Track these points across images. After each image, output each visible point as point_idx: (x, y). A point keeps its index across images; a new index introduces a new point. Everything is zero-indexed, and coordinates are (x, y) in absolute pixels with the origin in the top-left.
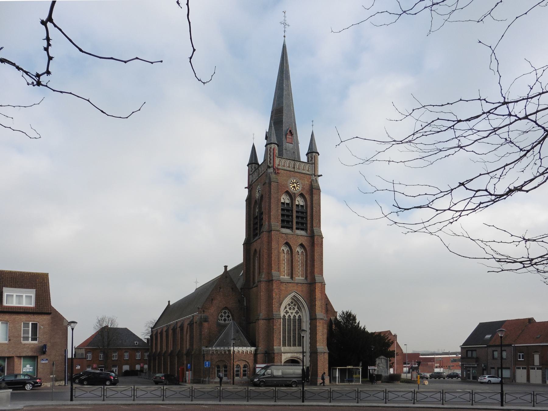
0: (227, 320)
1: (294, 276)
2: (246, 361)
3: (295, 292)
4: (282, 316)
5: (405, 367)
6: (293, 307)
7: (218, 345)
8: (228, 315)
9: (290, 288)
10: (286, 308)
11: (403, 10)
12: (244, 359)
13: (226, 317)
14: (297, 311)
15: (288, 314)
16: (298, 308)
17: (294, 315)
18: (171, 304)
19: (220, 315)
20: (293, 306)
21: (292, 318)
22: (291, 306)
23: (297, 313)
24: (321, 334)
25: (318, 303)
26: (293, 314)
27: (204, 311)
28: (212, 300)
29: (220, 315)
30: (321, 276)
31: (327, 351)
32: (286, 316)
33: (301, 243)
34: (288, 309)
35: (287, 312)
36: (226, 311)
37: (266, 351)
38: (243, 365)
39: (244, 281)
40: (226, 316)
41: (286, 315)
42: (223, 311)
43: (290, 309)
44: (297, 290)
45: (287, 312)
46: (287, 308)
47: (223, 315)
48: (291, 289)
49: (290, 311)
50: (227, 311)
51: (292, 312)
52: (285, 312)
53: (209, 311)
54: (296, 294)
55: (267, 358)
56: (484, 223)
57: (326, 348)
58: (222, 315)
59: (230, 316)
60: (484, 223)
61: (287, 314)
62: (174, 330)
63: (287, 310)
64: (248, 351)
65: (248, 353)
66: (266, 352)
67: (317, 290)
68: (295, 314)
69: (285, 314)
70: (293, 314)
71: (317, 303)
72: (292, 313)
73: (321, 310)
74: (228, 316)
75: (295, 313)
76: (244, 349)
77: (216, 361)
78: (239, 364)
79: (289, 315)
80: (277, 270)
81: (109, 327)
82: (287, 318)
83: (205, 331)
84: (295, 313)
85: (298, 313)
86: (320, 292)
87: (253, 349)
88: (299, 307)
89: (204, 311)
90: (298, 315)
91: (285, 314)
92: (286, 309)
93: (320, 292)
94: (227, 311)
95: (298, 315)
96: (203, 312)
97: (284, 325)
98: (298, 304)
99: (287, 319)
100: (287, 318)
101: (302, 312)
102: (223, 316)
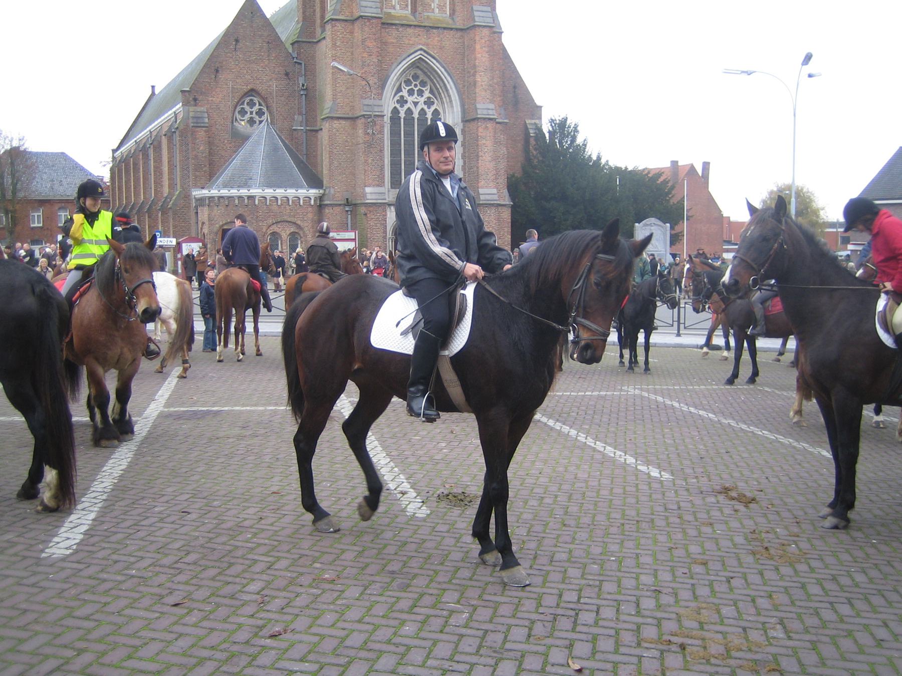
0: (258, 122)
1: (420, 9)
2: (295, 223)
3: (421, 49)
4: (388, 113)
5: (728, 251)
7: (226, 186)
8: (260, 109)
9: (409, 40)
10: (399, 90)
11: (552, 605)
12: (289, 219)
13: (254, 115)
14: (429, 98)
15: (406, 107)
16: (431, 92)
17: (422, 109)
18: (157, 92)
19: (238, 109)
20: (419, 87)
21: (416, 115)
22: (413, 87)
23: (429, 103)
24: (490, 158)
25: (482, 79)
26: (419, 107)
27: (195, 100)
28: (217, 71)
29: (238, 109)
30: (489, 9)
31: (507, 201)
34: (404, 93)
35: (402, 101)
36: (255, 99)
37: (347, 199)
38: (288, 233)
39: (300, 25)
40: (254, 113)
41: (400, 109)
42: (247, 100)
43: (411, 92)
44: (427, 45)
45: (402, 101)
46: (403, 90)
47: (247, 108)
48: (411, 42)
49: (410, 99)
50: (256, 100)
51: (416, 100)
52: (398, 101)
54: (426, 55)
55: (349, 216)
56: (727, 72)
57: (505, 192)
58: (243, 108)
59: (264, 113)
60: (727, 72)
61: (402, 106)
63: (402, 97)
64: (299, 199)
65: (299, 202)
66: (347, 202)
67: (478, 47)
68: (425, 107)
69: (398, 106)
70: (419, 107)
71: (478, 79)
72: (416, 104)
74: (260, 113)
75: (425, 103)
76: (291, 192)
77: (221, 223)
78: (278, 230)
79: (409, 109)
82: (402, 115)
83: (198, 149)
84: (425, 103)
85: (433, 103)
86: (486, 49)
87: (313, 192)
88: (434, 89)
89: (195, 100)
90: (433, 108)
91: (398, 106)
92: (400, 94)
93: (486, 49)
94: (256, 100)
95: (433, 108)
96: (192, 103)
97: (395, 133)
98: (432, 80)
99: (402, 120)
100: (402, 115)
101: (442, 103)
102: (246, 113)
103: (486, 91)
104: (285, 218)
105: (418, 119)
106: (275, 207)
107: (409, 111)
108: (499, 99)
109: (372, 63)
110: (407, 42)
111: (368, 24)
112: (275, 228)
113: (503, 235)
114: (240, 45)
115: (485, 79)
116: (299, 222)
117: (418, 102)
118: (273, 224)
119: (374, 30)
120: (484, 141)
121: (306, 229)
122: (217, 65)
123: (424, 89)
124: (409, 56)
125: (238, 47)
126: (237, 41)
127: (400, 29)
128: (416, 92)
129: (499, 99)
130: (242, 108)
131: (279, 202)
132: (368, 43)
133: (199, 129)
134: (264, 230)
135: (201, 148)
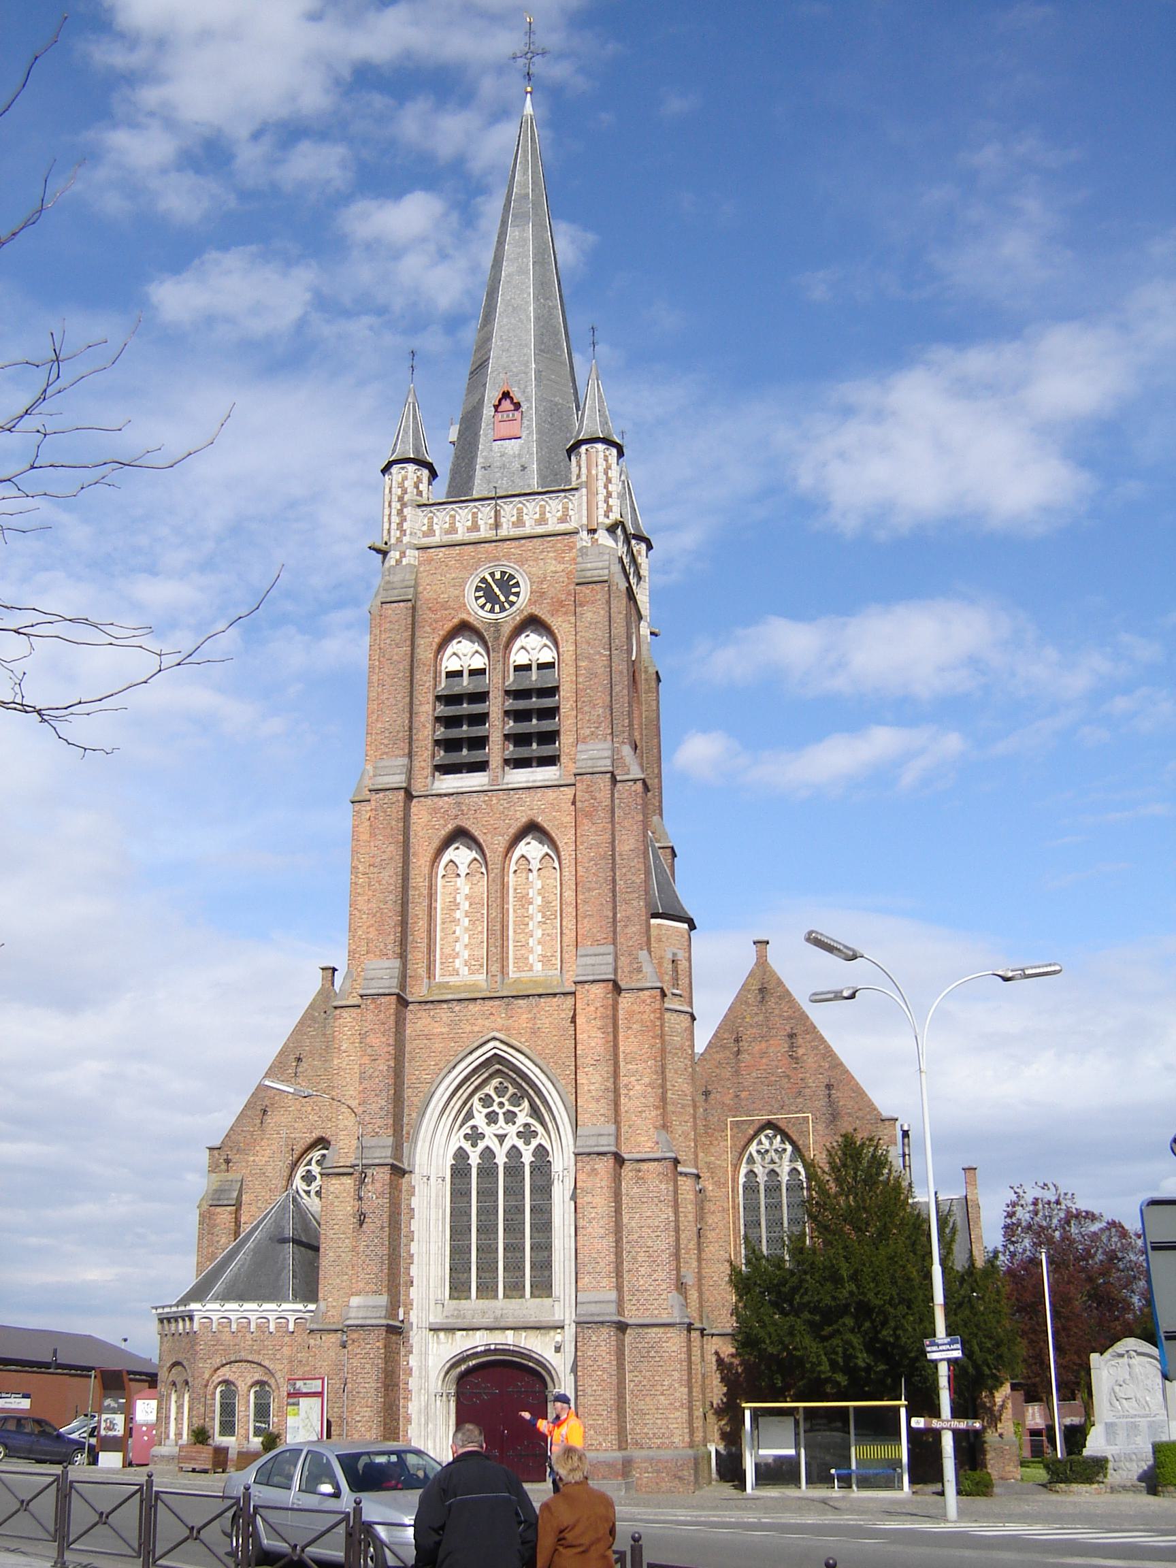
6: (509, 1111)
15: (481, 1145)
17: (514, 1147)
20: (508, 1107)
23: (527, 1134)
24: (602, 1231)
26: (508, 1144)
27: (227, 1161)
29: (301, 1171)
32: (524, 1153)
33: (524, 820)
34: (479, 1120)
43: (492, 1118)
45: (475, 1136)
48: (476, 1029)
49: (489, 1131)
51: (501, 1132)
53: (252, 1158)
62: (486, 1290)
68: (520, 1144)
70: (508, 1144)
72: (501, 1138)
73: (602, 1111)
75: (519, 1135)
80: (390, 952)
81: (958, 1354)
84: (519, 1135)
85: (535, 1134)
86: (599, 1023)
96: (224, 1167)
100: (474, 1160)
103: (598, 1101)
104: (244, 1355)
105: (506, 1167)
106: (226, 1337)
107: (488, 1153)
108: (654, 1113)
109: (376, 1073)
110: (468, 1028)
111: (372, 1006)
112: (225, 1373)
113: (670, 1386)
114: (304, 1065)
115: (597, 1078)
116: (266, 1363)
117: (505, 1136)
118: (223, 1366)
119: (382, 1016)
120: (588, 1199)
121: (278, 1375)
122: (267, 1102)
123: (515, 1110)
124: (471, 1053)
125: (300, 1069)
126: (299, 1060)
127: (457, 1008)
128: (501, 1117)
129: (654, 1113)
130: (309, 1171)
131: (234, 1327)
132: (373, 1040)
133: (219, 1209)
134: (207, 1376)
135: (223, 1240)
